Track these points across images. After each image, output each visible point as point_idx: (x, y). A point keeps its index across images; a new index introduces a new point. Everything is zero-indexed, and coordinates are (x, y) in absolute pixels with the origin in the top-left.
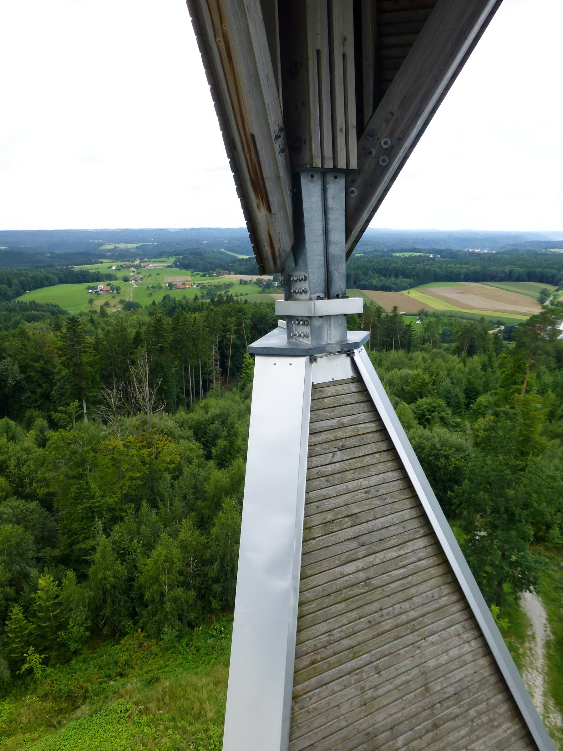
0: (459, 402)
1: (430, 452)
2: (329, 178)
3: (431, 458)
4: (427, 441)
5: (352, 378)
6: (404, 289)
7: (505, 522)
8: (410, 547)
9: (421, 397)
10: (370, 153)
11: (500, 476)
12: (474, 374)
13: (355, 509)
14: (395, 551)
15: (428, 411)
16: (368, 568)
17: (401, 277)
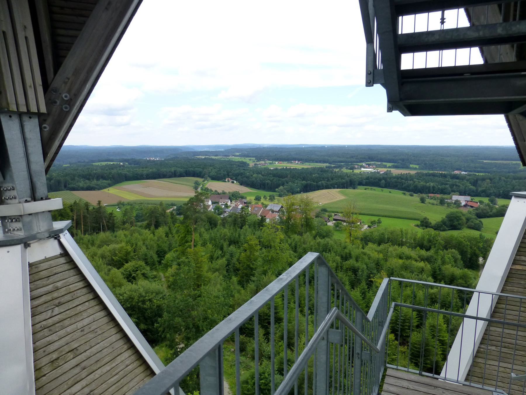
0: (154, 261)
1: (138, 300)
2: (25, 118)
3: (139, 304)
4: (135, 292)
5: (61, 254)
6: (105, 187)
7: (194, 333)
8: (119, 359)
9: (127, 262)
10: (56, 102)
11: (186, 304)
12: (161, 240)
13: (74, 345)
14: (109, 366)
15: (133, 271)
16: (90, 384)
17: (101, 180)
